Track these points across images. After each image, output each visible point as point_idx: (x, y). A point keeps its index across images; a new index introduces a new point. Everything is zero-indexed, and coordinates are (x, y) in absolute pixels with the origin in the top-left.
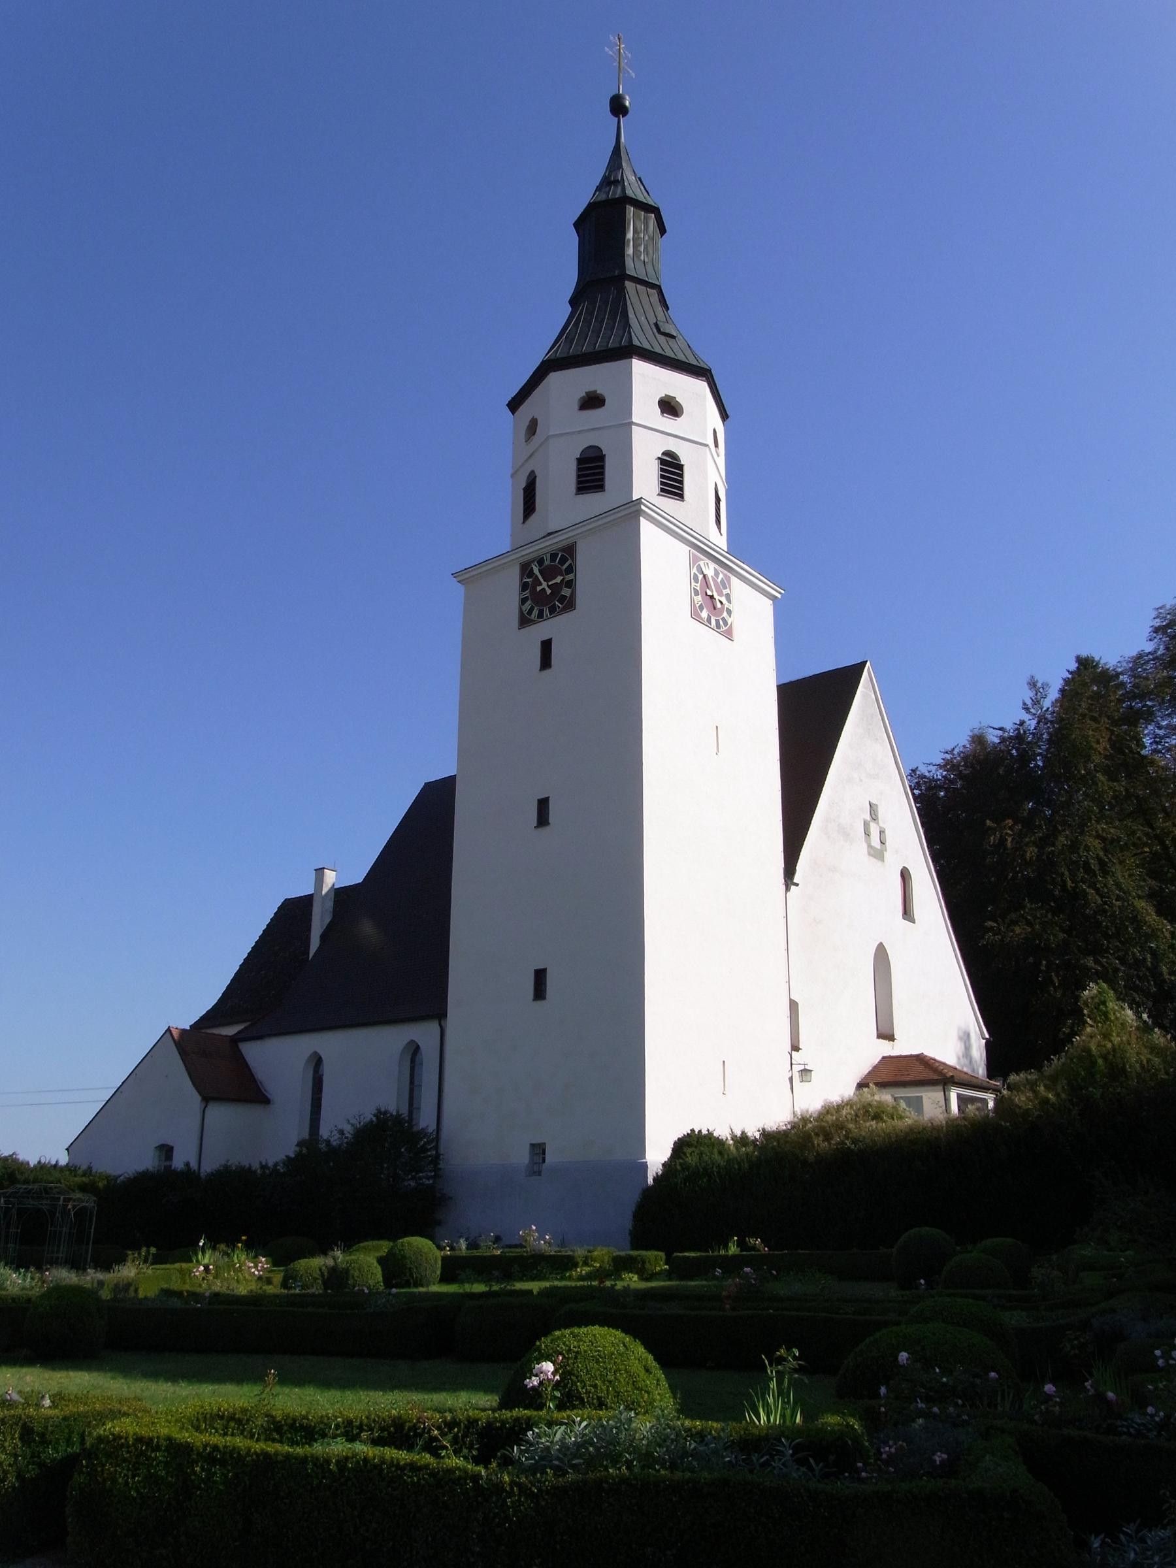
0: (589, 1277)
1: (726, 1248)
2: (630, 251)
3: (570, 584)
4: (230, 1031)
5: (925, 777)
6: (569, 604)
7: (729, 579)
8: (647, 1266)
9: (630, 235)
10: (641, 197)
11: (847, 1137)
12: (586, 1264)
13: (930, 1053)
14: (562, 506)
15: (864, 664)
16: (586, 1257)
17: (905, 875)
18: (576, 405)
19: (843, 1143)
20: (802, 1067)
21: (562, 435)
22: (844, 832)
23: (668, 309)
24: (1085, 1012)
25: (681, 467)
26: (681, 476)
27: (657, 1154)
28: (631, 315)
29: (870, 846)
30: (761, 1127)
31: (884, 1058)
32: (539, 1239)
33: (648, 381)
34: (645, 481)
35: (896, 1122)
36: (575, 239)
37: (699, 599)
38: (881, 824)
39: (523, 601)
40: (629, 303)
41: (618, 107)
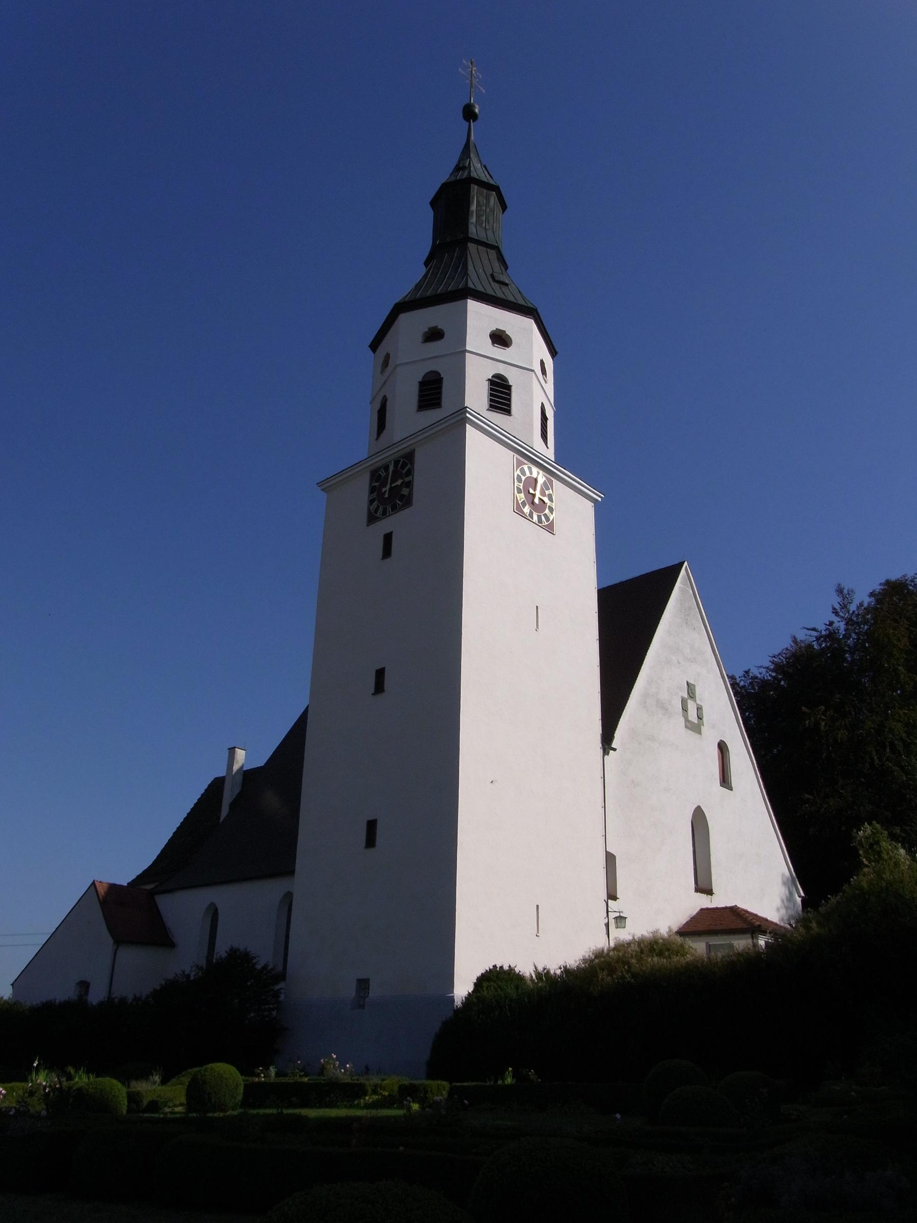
0: (374, 1105)
1: (503, 1079)
2: (473, 219)
3: (409, 485)
4: (149, 887)
5: (757, 678)
6: (407, 502)
7: (551, 483)
8: (429, 1095)
9: (474, 207)
10: (484, 177)
11: (628, 971)
12: (375, 1092)
13: (743, 905)
14: (406, 419)
15: (682, 564)
16: (376, 1086)
17: (722, 747)
18: (419, 338)
19: (623, 977)
20: (618, 914)
21: (408, 363)
22: (663, 707)
23: (506, 268)
24: (861, 852)
25: (509, 388)
26: (510, 395)
27: (462, 988)
28: (470, 267)
29: (687, 720)
30: (562, 963)
31: (702, 910)
32: (340, 1067)
33: (481, 318)
34: (476, 396)
35: (675, 959)
36: (430, 213)
37: (521, 497)
38: (698, 702)
39: (371, 502)
40: (469, 256)
41: (469, 114)
